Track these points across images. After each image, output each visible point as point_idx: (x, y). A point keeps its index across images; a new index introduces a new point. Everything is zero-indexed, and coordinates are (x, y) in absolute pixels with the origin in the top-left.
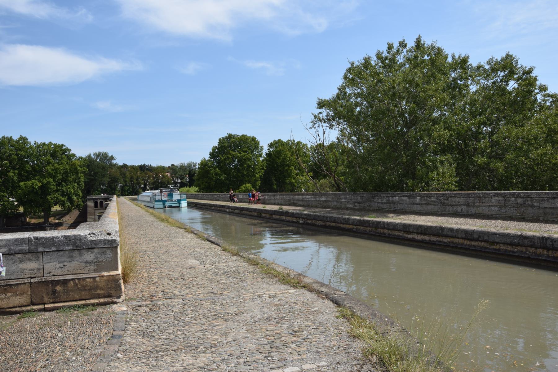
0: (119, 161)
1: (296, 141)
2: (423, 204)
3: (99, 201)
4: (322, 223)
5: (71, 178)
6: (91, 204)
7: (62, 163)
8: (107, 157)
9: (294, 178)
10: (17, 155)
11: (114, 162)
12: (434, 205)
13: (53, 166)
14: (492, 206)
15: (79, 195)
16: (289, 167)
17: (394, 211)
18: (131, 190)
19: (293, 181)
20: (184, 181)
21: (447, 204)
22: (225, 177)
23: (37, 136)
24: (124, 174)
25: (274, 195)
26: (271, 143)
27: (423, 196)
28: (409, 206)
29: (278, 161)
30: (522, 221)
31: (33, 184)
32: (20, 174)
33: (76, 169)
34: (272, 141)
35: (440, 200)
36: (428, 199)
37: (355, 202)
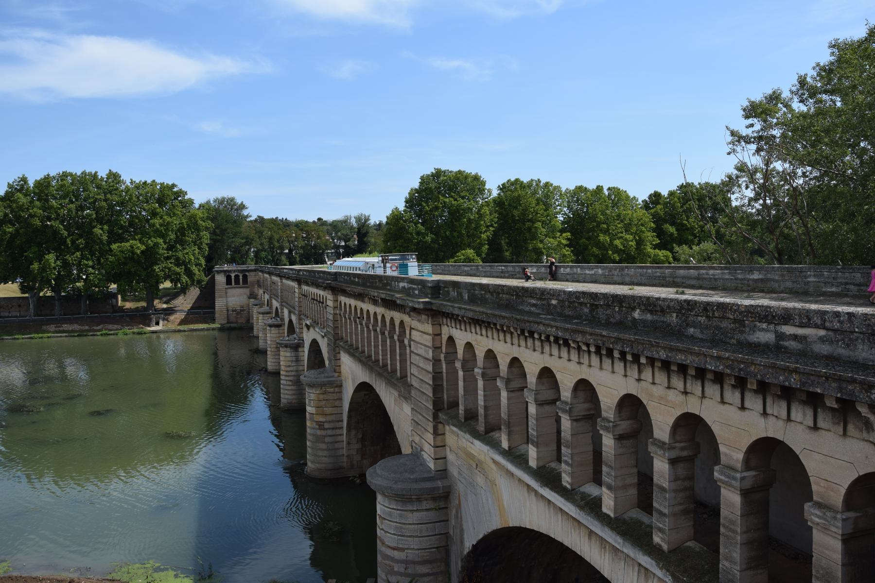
0: (253, 212)
1: (543, 181)
3: (233, 275)
5: (190, 237)
6: (220, 279)
7: (174, 214)
8: (235, 204)
9: (542, 241)
10: (106, 200)
11: (245, 212)
13: (161, 218)
15: (200, 265)
16: (534, 223)
18: (270, 257)
19: (541, 246)
20: (350, 243)
22: (432, 239)
23: (135, 171)
24: (261, 233)
25: (622, 269)
26: (503, 185)
29: (516, 213)
31: (132, 247)
32: (111, 232)
33: (196, 223)
34: (505, 181)
37: (846, 284)
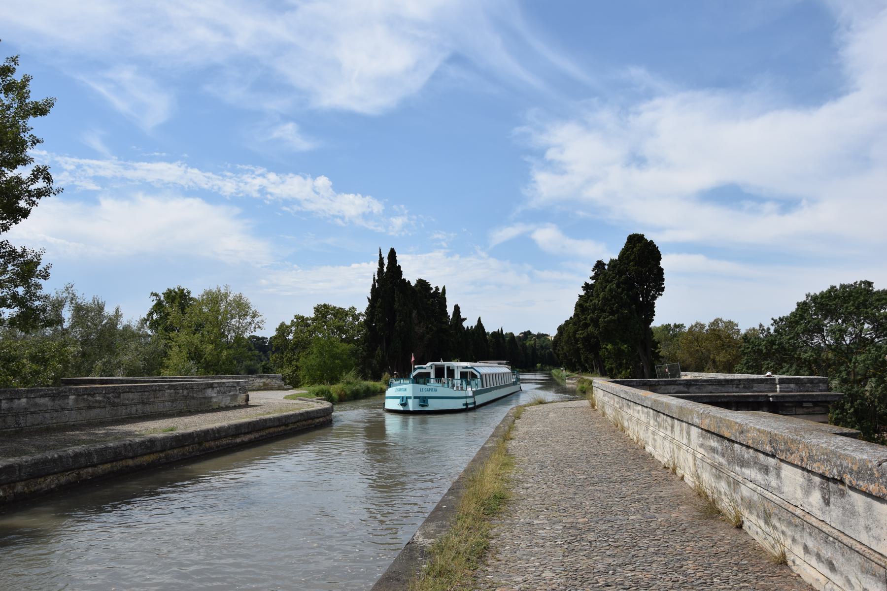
2: (82, 408)
4: (71, 476)
12: (100, 407)
14: (166, 401)
17: (17, 432)
21: (119, 405)
27: (78, 394)
28: (55, 415)
35: (109, 398)
36: (90, 398)
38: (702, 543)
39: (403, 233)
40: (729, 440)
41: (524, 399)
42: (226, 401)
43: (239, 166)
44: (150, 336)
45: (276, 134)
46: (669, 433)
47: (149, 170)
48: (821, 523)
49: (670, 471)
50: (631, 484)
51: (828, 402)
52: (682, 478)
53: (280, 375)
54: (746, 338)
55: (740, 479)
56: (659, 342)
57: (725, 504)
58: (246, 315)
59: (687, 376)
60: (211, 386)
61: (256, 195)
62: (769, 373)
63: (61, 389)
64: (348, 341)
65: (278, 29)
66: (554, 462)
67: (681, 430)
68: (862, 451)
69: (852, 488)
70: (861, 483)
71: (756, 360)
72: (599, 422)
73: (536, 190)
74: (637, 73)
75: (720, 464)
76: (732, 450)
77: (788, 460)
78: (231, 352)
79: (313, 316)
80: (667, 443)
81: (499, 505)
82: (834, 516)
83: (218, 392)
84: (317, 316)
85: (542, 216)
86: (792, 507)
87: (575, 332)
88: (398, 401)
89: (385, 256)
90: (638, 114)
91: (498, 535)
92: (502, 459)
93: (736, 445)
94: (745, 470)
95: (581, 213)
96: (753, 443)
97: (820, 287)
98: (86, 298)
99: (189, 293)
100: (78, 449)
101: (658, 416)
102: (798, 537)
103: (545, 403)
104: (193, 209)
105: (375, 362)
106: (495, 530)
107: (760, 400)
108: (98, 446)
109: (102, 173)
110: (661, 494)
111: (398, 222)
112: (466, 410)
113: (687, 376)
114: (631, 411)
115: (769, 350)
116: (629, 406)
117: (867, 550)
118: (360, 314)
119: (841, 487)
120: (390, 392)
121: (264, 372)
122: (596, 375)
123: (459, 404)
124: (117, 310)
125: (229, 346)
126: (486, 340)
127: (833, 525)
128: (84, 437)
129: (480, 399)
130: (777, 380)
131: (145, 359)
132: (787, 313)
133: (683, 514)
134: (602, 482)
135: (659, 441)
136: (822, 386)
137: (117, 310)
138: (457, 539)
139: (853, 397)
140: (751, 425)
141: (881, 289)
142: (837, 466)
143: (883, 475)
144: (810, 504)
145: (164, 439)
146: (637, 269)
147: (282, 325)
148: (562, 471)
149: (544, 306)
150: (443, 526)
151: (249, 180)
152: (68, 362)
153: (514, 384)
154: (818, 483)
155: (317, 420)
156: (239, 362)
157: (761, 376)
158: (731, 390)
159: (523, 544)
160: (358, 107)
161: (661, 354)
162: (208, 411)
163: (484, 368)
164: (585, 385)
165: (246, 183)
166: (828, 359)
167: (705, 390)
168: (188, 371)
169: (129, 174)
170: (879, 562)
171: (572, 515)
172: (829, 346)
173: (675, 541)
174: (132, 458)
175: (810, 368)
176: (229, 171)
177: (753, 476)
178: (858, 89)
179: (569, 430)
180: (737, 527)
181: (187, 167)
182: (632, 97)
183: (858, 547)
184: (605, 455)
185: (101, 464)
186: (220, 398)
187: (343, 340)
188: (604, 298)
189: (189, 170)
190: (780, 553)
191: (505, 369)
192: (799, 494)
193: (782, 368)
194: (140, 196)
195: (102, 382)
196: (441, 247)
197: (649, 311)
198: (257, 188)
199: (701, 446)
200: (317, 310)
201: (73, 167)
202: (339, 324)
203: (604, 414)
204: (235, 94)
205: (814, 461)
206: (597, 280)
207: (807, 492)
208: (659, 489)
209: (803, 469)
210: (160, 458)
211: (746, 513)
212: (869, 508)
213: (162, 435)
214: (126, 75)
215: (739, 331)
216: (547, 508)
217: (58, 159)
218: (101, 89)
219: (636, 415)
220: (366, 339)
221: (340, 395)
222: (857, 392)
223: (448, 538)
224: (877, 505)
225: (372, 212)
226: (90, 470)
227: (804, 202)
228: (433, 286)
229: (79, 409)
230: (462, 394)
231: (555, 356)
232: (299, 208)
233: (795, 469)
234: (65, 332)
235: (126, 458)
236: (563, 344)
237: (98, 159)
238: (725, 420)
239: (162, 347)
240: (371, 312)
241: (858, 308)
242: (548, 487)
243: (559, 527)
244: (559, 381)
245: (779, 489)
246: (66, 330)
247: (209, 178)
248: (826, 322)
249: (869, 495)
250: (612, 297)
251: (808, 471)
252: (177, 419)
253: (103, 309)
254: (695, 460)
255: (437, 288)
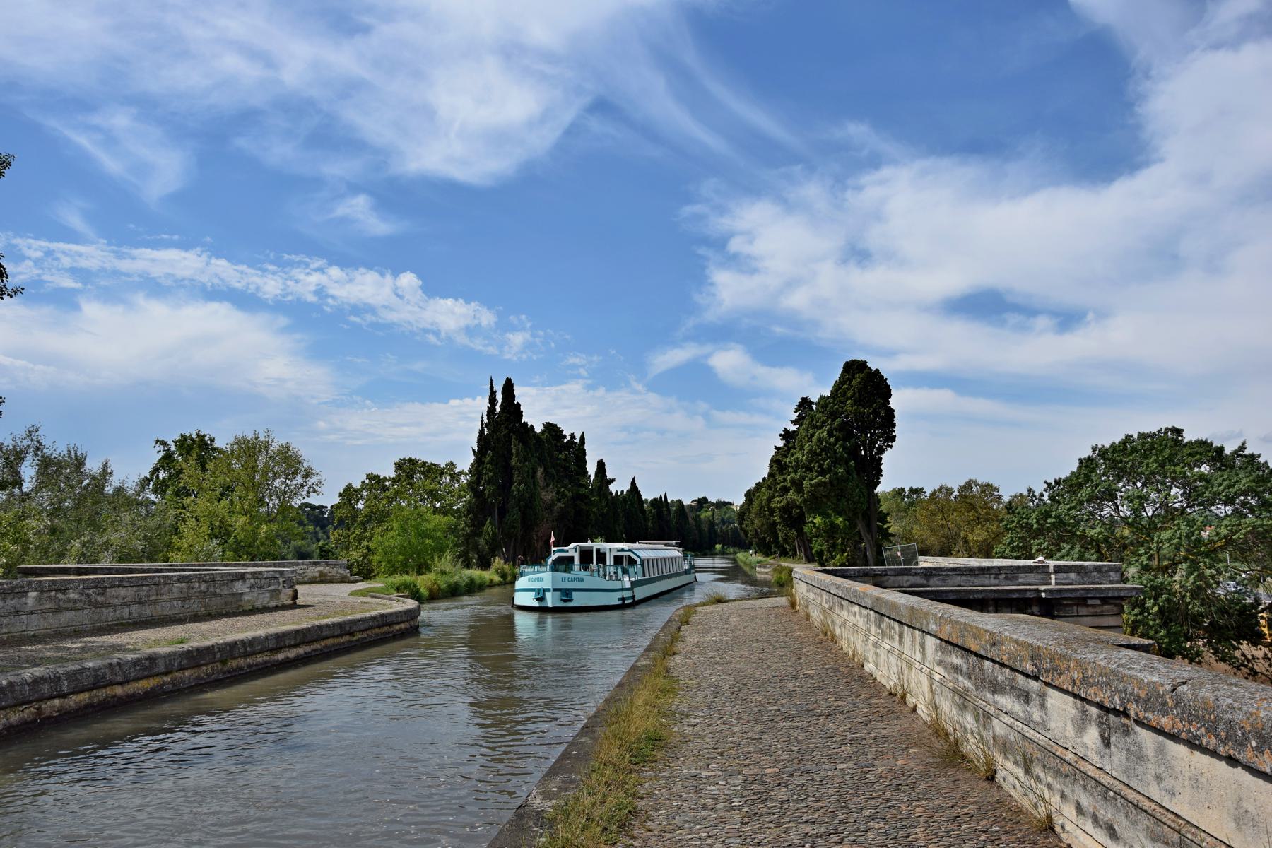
2: (48, 611)
4: (27, 713)
12: (75, 609)
21: (103, 605)
30: (196, 621)
35: (88, 596)
36: (60, 596)
38: (937, 802)
39: (524, 356)
40: (977, 655)
41: (698, 596)
42: (264, 599)
43: (286, 256)
44: (154, 503)
45: (341, 210)
46: (896, 645)
47: (153, 260)
48: (1099, 772)
49: (897, 699)
50: (842, 718)
51: (1122, 598)
52: (914, 710)
53: (344, 561)
54: (1010, 507)
55: (992, 710)
56: (888, 514)
57: (971, 747)
58: (295, 473)
59: (926, 562)
60: (242, 577)
61: (311, 298)
62: (1041, 558)
63: (15, 582)
64: (444, 511)
65: (344, 58)
66: (734, 686)
67: (913, 641)
68: (1152, 670)
69: (1138, 722)
70: (1150, 715)
71: (1023, 539)
72: (801, 629)
73: (714, 295)
74: (857, 131)
75: (966, 690)
76: (981, 669)
77: (1056, 684)
78: (274, 527)
79: (393, 475)
80: (893, 659)
81: (653, 750)
82: (1115, 761)
83: (252, 586)
84: (399, 476)
85: (723, 333)
86: (1060, 749)
87: (769, 500)
88: (533, 594)
89: (499, 388)
90: (859, 188)
91: (650, 794)
92: (661, 682)
93: (987, 663)
94: (997, 697)
95: (778, 330)
96: (1009, 659)
97: (1111, 436)
98: (57, 446)
99: (212, 440)
100: (39, 671)
101: (881, 621)
102: (1068, 792)
103: (726, 602)
104: (217, 318)
105: (482, 542)
106: (646, 786)
107: (1028, 595)
108: (71, 667)
109: (83, 263)
110: (884, 732)
111: (517, 339)
112: (622, 606)
113: (926, 562)
114: (844, 614)
115: (1042, 525)
116: (842, 606)
117: (1158, 809)
118: (461, 473)
119: (1125, 721)
120: (520, 583)
121: (322, 557)
122: (799, 561)
123: (613, 599)
124: (105, 466)
125: (270, 519)
126: (643, 511)
127: (1114, 774)
128: (49, 654)
129: (641, 593)
130: (1053, 570)
131: (145, 537)
132: (1064, 474)
133: (912, 761)
134: (800, 715)
135: (883, 656)
136: (1114, 576)
137: (105, 466)
138: (589, 801)
139: (1157, 591)
140: (1007, 633)
141: (1194, 439)
142: (1119, 692)
143: (1178, 704)
144: (1085, 745)
145: (170, 655)
146: (859, 409)
147: (349, 487)
148: (744, 700)
149: (726, 463)
150: (572, 782)
151: (302, 277)
152: (28, 541)
153: (687, 572)
154: (1095, 716)
155: (397, 627)
156: (285, 542)
157: (1030, 563)
158: (987, 582)
159: (685, 807)
160: (460, 174)
161: (891, 530)
162: (236, 614)
163: (645, 550)
164: (784, 575)
165: (297, 282)
166: (1122, 537)
167: (951, 582)
168: (210, 555)
169: (124, 265)
170: (1173, 825)
171: (756, 764)
172: (1125, 519)
173: (900, 800)
174: (121, 684)
175: (1098, 551)
176: (272, 263)
177: (1009, 706)
178: (1162, 160)
179: (757, 641)
180: (987, 779)
181: (210, 257)
182: (851, 165)
183: (1146, 804)
184: (807, 676)
185: (73, 693)
186: (255, 594)
187: (436, 511)
188: (810, 451)
189: (213, 261)
190: (1044, 816)
191: (675, 553)
192: (1070, 731)
193: (1059, 550)
194: (140, 299)
195: (79, 571)
196: (579, 377)
197: (873, 470)
198: (313, 288)
199: (940, 663)
200: (399, 466)
201: (39, 254)
202: (431, 487)
203: (808, 617)
204: (280, 152)
205: (1090, 685)
206: (801, 425)
207: (1081, 729)
208: (880, 725)
209: (1076, 696)
210: (164, 684)
211: (1000, 759)
212: (1161, 750)
213: (166, 650)
214: (121, 120)
215: (1000, 497)
216: (721, 754)
217: (17, 241)
218: (83, 140)
219: (851, 618)
220: (470, 509)
221: (431, 590)
222: (1162, 583)
223: (576, 799)
224: (1170, 744)
225: (479, 326)
226: (57, 702)
227: (1090, 316)
228: (567, 433)
229: (43, 612)
230: (617, 585)
231: (742, 533)
232: (374, 318)
233: (1065, 696)
234: (26, 497)
235: (112, 684)
236: (752, 516)
237: (77, 243)
238: (971, 626)
239: (171, 520)
240: (477, 469)
241: (1162, 466)
242: (725, 723)
243: (737, 781)
244: (747, 569)
245: (1043, 724)
246: (27, 494)
247: (242, 272)
248: (1120, 485)
249: (1160, 731)
250: (822, 450)
251: (1083, 699)
252: (190, 626)
253: (83, 463)
254: (931, 684)
255: (573, 436)
